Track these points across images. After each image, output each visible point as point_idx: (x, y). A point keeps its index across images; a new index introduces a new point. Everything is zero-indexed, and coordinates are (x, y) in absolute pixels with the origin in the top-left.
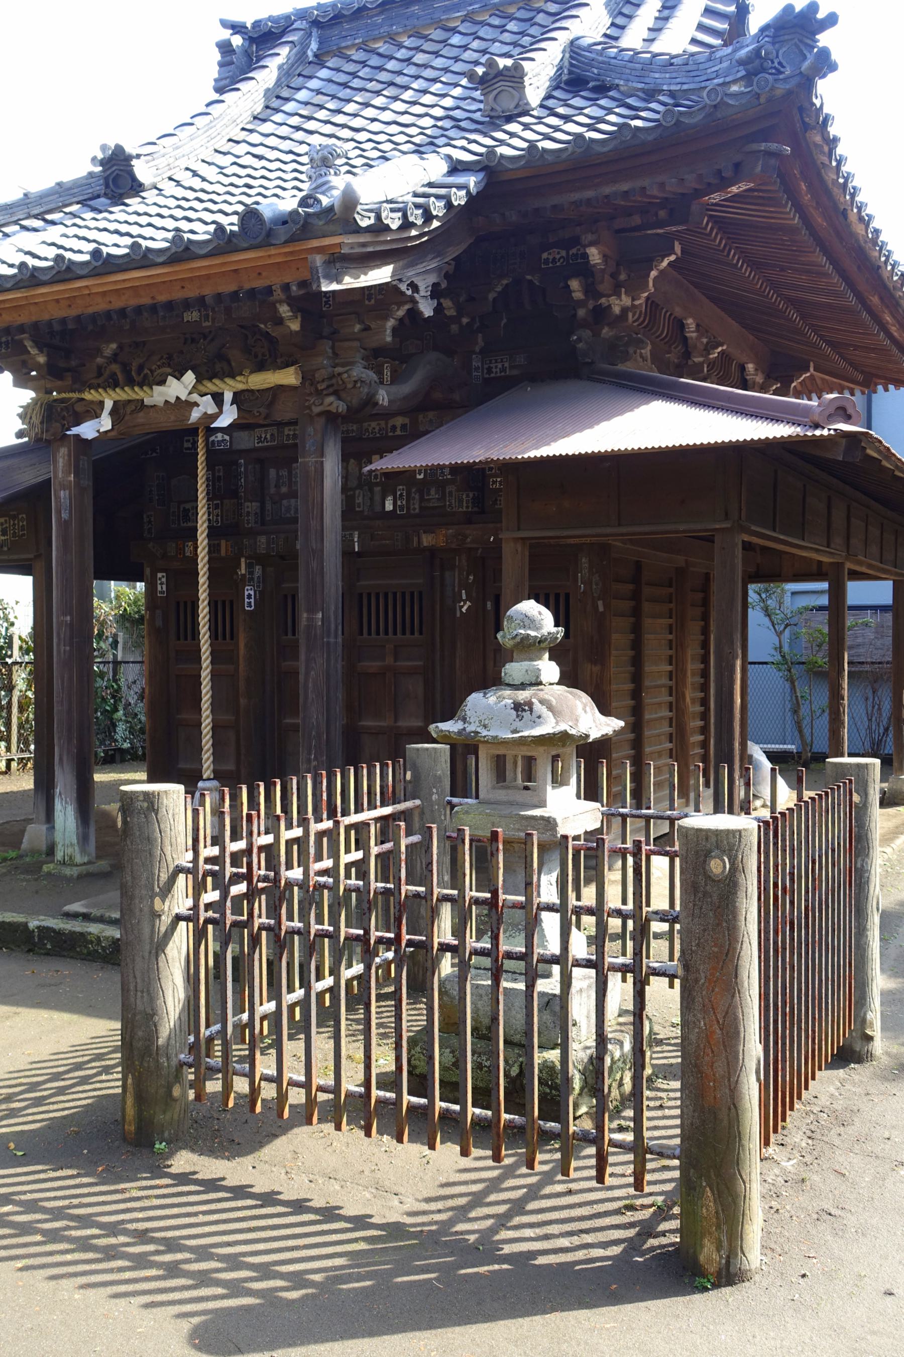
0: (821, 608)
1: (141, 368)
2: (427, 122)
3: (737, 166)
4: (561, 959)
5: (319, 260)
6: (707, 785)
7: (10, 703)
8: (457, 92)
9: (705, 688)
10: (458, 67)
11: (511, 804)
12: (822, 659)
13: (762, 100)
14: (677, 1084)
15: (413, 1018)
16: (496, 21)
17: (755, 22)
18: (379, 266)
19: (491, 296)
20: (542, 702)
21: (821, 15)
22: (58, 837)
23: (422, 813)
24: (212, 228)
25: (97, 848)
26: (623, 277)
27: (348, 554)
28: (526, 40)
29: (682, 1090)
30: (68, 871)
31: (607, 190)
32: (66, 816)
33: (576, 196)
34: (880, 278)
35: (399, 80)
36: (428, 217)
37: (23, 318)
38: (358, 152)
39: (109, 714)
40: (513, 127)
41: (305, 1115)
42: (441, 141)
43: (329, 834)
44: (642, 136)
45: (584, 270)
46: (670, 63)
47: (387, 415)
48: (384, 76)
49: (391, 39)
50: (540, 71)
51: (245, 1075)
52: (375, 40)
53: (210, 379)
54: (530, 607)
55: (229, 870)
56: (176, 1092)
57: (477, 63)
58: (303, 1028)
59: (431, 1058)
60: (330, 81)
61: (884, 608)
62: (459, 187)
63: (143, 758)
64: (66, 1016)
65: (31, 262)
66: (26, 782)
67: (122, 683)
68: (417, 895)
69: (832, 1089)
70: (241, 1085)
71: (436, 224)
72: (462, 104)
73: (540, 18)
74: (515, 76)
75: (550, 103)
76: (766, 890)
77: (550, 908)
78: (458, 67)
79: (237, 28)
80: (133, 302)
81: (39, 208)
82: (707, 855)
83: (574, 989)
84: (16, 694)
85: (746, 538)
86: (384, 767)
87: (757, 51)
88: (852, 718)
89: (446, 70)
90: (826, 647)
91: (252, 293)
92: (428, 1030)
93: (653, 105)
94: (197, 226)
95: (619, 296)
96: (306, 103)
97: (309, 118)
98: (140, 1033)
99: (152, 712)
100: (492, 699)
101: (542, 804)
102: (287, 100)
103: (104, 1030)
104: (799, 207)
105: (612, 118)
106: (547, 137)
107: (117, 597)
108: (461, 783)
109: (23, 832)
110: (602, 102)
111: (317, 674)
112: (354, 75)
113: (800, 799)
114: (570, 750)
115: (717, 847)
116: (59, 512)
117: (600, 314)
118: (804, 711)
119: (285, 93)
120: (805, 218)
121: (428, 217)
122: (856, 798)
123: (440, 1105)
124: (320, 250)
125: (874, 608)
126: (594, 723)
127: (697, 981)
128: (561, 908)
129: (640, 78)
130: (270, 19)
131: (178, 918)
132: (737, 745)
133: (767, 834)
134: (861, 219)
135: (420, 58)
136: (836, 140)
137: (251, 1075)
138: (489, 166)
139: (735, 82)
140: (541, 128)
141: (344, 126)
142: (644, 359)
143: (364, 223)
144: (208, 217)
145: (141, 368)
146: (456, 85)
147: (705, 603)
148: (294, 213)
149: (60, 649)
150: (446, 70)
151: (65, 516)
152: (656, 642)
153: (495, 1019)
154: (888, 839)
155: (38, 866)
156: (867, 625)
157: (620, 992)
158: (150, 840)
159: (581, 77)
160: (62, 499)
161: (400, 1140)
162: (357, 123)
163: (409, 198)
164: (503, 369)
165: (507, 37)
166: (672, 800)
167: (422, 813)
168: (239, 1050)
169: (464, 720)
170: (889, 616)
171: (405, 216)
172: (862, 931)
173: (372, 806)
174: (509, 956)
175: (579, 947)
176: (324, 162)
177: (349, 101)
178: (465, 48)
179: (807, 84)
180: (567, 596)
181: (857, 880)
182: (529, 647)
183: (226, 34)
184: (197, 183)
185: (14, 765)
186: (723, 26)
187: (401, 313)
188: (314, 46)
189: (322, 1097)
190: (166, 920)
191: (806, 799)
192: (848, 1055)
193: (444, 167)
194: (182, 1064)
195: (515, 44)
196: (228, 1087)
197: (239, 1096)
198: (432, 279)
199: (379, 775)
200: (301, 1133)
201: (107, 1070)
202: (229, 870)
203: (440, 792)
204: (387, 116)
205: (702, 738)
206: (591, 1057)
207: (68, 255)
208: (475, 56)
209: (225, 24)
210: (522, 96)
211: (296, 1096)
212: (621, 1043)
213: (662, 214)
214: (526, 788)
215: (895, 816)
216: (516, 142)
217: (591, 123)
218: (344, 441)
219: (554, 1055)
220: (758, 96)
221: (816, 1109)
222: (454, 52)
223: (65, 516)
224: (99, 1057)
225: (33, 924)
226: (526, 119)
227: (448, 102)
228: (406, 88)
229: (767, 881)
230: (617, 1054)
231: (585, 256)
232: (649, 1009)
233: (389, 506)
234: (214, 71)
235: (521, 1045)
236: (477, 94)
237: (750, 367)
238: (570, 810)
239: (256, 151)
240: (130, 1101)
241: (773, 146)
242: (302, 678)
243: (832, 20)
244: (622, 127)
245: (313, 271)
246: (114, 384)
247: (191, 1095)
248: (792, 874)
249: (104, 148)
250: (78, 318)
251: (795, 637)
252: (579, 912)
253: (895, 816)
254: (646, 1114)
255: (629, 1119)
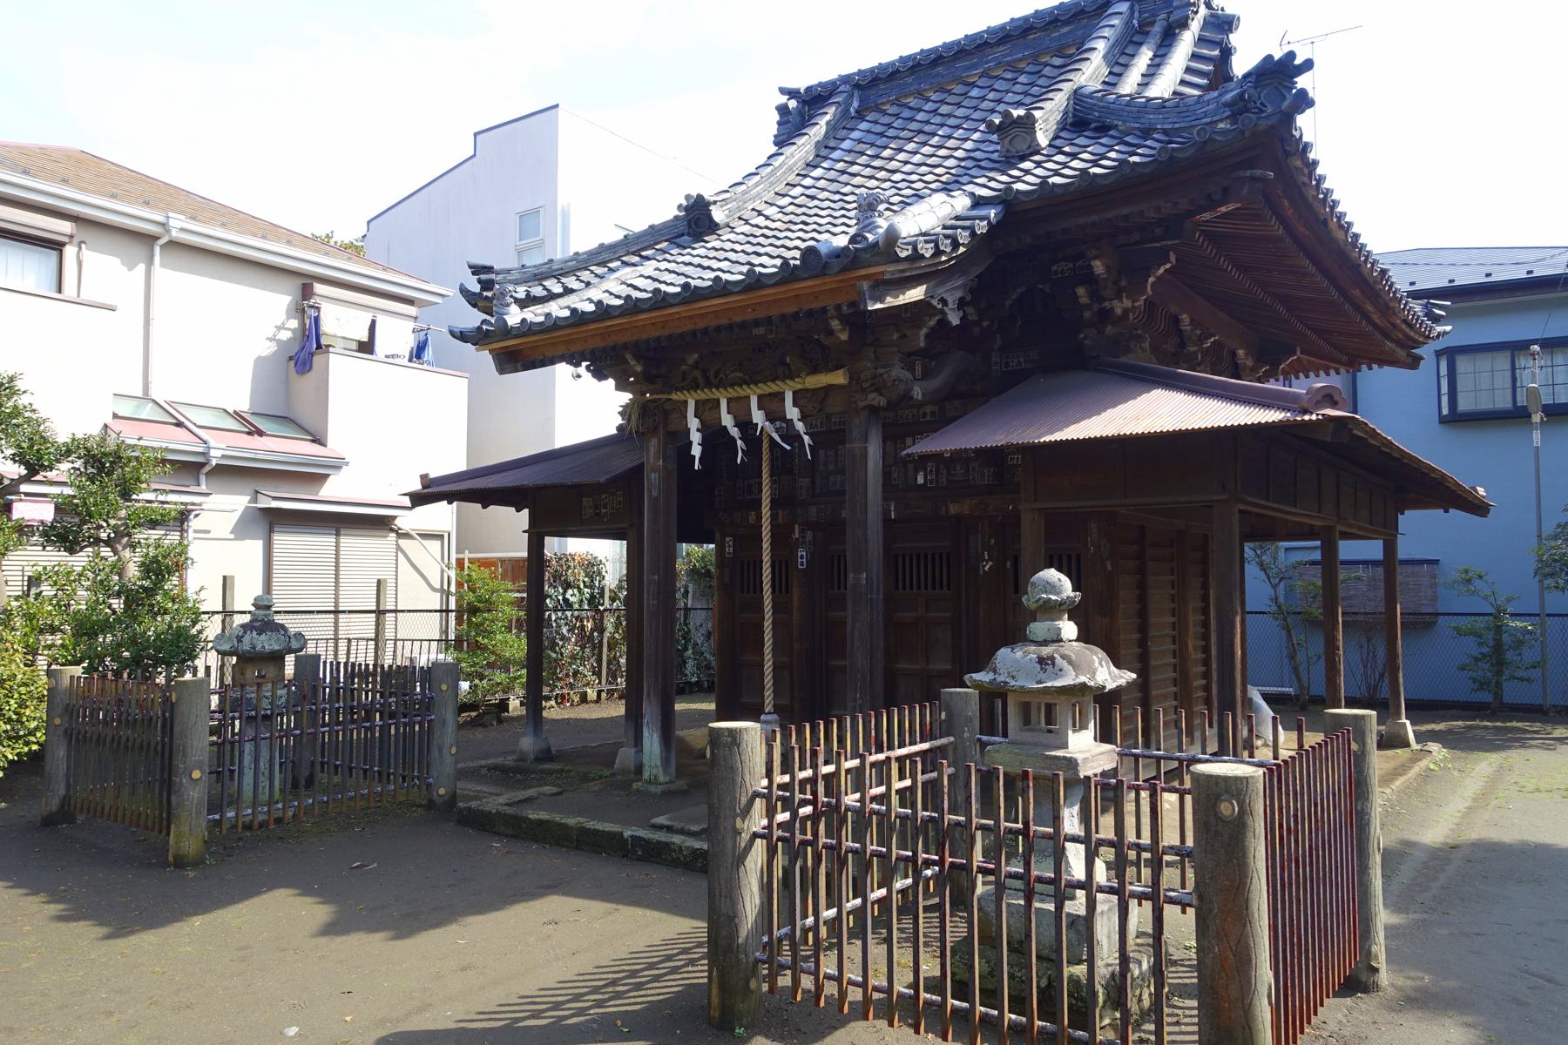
0: (1313, 563)
1: (717, 374)
2: (951, 162)
3: (1225, 190)
4: (1087, 884)
5: (865, 285)
6: (1211, 726)
7: (601, 642)
8: (976, 136)
9: (1206, 637)
10: (977, 115)
11: (1036, 744)
12: (1317, 611)
13: (1247, 134)
14: (1195, 1003)
15: (956, 930)
16: (1009, 75)
17: (1241, 65)
18: (915, 287)
19: (1007, 303)
20: (1063, 657)
21: (1298, 62)
22: (646, 760)
23: (956, 748)
24: (778, 262)
25: (677, 769)
26: (1124, 283)
27: (887, 521)
28: (1035, 90)
29: (1199, 1008)
30: (653, 789)
31: (1110, 214)
32: (652, 742)
33: (1082, 220)
34: (1360, 274)
35: (927, 128)
36: (956, 244)
37: (626, 338)
38: (894, 191)
39: (681, 653)
40: (1027, 165)
41: (862, 1011)
42: (965, 179)
43: (879, 766)
44: (1139, 170)
45: (1089, 279)
46: (1163, 105)
47: (920, 405)
48: (914, 126)
49: (920, 94)
50: (1048, 117)
51: (810, 973)
52: (906, 96)
53: (773, 381)
54: (1052, 574)
55: (798, 796)
56: (753, 984)
57: (993, 111)
58: (859, 932)
59: (972, 967)
60: (868, 131)
61: (1375, 563)
62: (982, 219)
63: (710, 690)
64: (657, 914)
65: (636, 294)
66: (618, 709)
67: (691, 626)
68: (958, 824)
69: (1340, 1016)
70: (807, 982)
71: (962, 249)
72: (982, 146)
73: (1047, 71)
74: (1028, 123)
75: (1058, 142)
76: (1273, 830)
77: (1075, 839)
78: (977, 115)
79: (792, 93)
80: (714, 323)
81: (635, 246)
82: (1218, 798)
83: (1099, 908)
84: (607, 634)
85: (1242, 507)
86: (922, 708)
87: (1241, 95)
88: (1347, 664)
89: (967, 118)
90: (1320, 598)
91: (810, 313)
92: (968, 940)
93: (1149, 143)
94: (765, 260)
95: (1121, 300)
96: (850, 151)
97: (853, 163)
98: (724, 933)
99: (720, 652)
100: (1019, 654)
101: (1065, 746)
102: (834, 149)
103: (691, 928)
104: (1282, 220)
105: (1113, 155)
106: (1057, 173)
107: (693, 553)
108: (991, 721)
109: (615, 755)
110: (1103, 141)
111: (862, 626)
112: (889, 126)
113: (1301, 746)
114: (1089, 699)
115: (1227, 792)
116: (650, 491)
117: (1104, 316)
118: (1301, 657)
119: (832, 144)
120: (1288, 229)
121: (956, 244)
122: (1354, 746)
123: (951, 1002)
124: (866, 277)
125: (1365, 563)
126: (1108, 675)
127: (1210, 911)
128: (1085, 840)
129: (1136, 119)
130: (820, 84)
131: (755, 835)
132: (1238, 692)
133: (1271, 780)
134: (1341, 227)
135: (944, 109)
136: (1315, 163)
137: (816, 973)
138: (1007, 200)
139: (1221, 120)
140: (1050, 165)
141: (881, 169)
142: (1144, 350)
143: (903, 255)
144: (774, 251)
145: (717, 374)
146: (976, 130)
147: (1204, 561)
148: (846, 248)
149: (649, 601)
150: (967, 118)
151: (655, 493)
152: (1159, 597)
153: (1028, 936)
154: (1387, 779)
155: (629, 784)
156: (1358, 579)
157: (1139, 915)
158: (733, 769)
159: (1085, 119)
160: (652, 479)
161: (945, 1039)
162: (893, 165)
163: (939, 230)
164: (1019, 364)
165: (1018, 88)
166: (1180, 742)
167: (956, 748)
168: (805, 951)
169: (995, 671)
170: (1380, 570)
171: (937, 246)
172: (1364, 869)
173: (913, 743)
174: (1040, 880)
175: (1101, 875)
176: (868, 207)
177: (885, 147)
178: (983, 98)
179: (1288, 119)
180: (1078, 557)
181: (1358, 822)
182: (1052, 610)
183: (784, 99)
184: (761, 221)
185: (604, 695)
186: (1208, 68)
187: (932, 323)
188: (855, 104)
189: (876, 996)
190: (745, 837)
191: (1306, 747)
192: (1356, 984)
193: (967, 202)
194: (757, 961)
195: (1026, 94)
196: (796, 982)
197: (804, 991)
198: (959, 294)
199: (919, 715)
200: (858, 1027)
201: (692, 962)
202: (798, 796)
203: (972, 731)
204: (917, 159)
205: (1203, 682)
206: (1113, 974)
207: (663, 287)
208: (992, 105)
209: (783, 91)
210: (1034, 138)
211: (855, 994)
212: (1140, 963)
213: (1158, 231)
214: (1050, 731)
215: (1393, 758)
216: (1029, 178)
217: (1094, 160)
218: (884, 425)
219: (1080, 970)
220: (1242, 132)
221: (1325, 1034)
222: (974, 103)
223: (655, 493)
224: (685, 951)
225: (627, 834)
226: (1037, 158)
227: (969, 145)
228: (934, 134)
229: (1273, 822)
230: (1136, 972)
231: (1090, 267)
232: (1166, 935)
233: (920, 480)
234: (774, 129)
235: (1051, 960)
236: (995, 137)
237: (1241, 352)
238: (1086, 749)
239: (808, 192)
240: (715, 991)
241: (1258, 172)
242: (849, 628)
243: (1308, 65)
244: (1123, 162)
245: (861, 294)
246: (695, 387)
247: (765, 987)
248: (1296, 816)
249: (688, 197)
250: (670, 337)
251: (1290, 591)
252: (1101, 843)
253: (1393, 758)
254: (1167, 1029)
255: (1150, 1033)
